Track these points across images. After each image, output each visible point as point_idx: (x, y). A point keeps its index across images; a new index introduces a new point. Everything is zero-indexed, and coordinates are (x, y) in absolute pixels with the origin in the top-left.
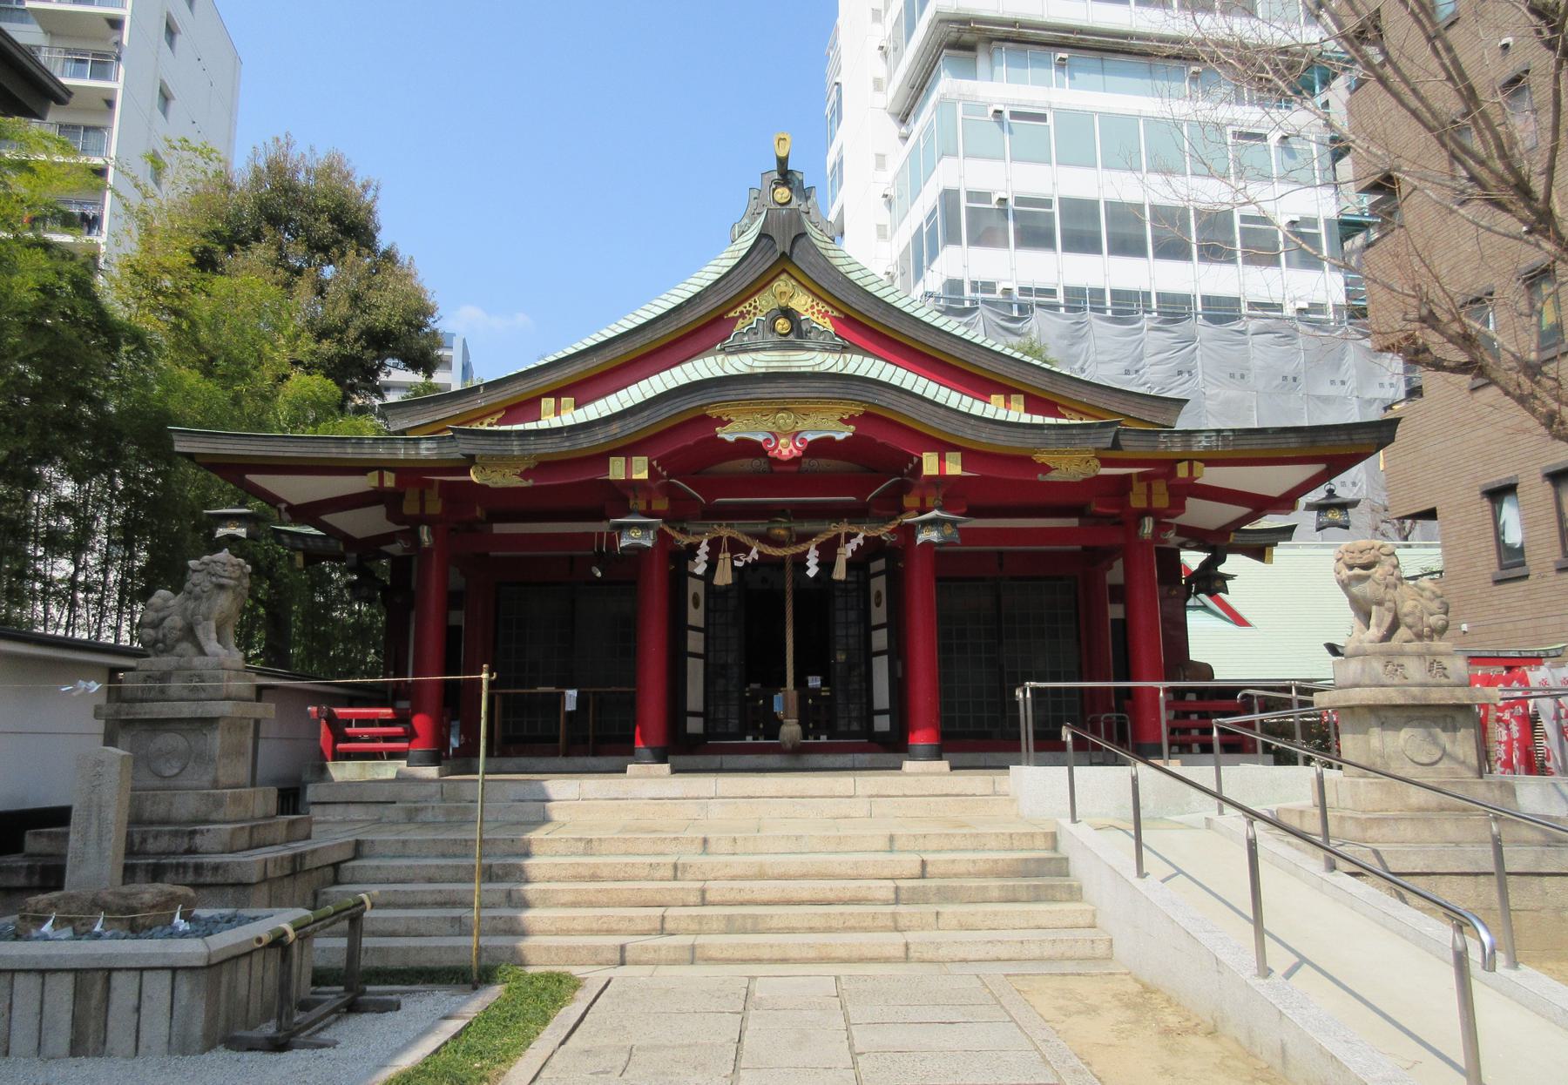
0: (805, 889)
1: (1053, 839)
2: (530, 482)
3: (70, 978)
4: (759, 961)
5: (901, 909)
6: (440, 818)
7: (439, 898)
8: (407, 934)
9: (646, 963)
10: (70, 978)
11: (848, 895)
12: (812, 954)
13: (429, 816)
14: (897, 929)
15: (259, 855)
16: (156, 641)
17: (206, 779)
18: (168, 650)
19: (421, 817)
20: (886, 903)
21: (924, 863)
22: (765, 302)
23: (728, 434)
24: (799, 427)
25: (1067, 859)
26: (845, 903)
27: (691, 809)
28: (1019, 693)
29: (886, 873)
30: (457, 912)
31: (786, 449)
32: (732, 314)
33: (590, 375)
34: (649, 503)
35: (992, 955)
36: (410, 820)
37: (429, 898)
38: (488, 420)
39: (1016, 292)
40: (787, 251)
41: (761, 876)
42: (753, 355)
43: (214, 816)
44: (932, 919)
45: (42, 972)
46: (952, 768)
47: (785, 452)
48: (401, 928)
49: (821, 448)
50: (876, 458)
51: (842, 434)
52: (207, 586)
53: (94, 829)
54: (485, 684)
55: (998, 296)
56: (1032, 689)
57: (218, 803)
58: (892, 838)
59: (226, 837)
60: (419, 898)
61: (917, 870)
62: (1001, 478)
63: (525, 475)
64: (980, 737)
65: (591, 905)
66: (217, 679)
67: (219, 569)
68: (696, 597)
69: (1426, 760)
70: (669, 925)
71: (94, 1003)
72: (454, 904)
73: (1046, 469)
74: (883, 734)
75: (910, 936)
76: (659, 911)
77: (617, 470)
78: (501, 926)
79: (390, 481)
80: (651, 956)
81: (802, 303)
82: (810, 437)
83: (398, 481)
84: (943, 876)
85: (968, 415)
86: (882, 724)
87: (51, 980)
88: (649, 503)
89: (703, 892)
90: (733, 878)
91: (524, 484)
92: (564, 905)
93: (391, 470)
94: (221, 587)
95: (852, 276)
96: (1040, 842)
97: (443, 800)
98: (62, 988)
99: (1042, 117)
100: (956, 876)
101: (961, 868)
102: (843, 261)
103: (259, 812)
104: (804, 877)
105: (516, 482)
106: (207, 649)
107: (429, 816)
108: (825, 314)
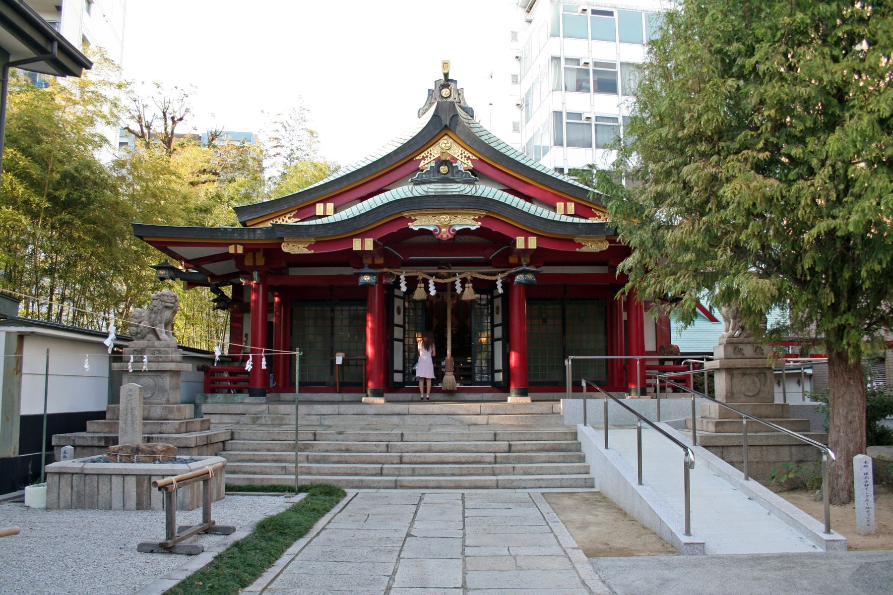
0: (452, 456)
1: (575, 435)
2: (312, 251)
3: (134, 478)
4: (427, 488)
5: (497, 466)
6: (269, 422)
7: (275, 458)
8: (261, 473)
9: (374, 488)
10: (134, 478)
11: (471, 460)
12: (452, 485)
13: (263, 421)
14: (494, 475)
15: (193, 435)
16: (137, 333)
17: (164, 399)
18: (143, 338)
19: (259, 422)
20: (490, 463)
21: (510, 445)
22: (435, 152)
23: (414, 226)
24: (453, 222)
25: (580, 443)
26: (470, 463)
27: (396, 420)
28: (566, 362)
29: (491, 449)
30: (283, 464)
31: (445, 234)
32: (418, 158)
33: (345, 188)
34: (373, 261)
35: (538, 485)
36: (254, 423)
37: (269, 458)
38: (288, 215)
39: (593, 119)
40: (448, 124)
41: (430, 451)
42: (428, 186)
43: (169, 417)
44: (511, 470)
45: (124, 475)
46: (533, 401)
47: (445, 236)
48: (258, 471)
49: (466, 232)
50: (490, 242)
51: (475, 226)
52: (160, 307)
53: (130, 419)
54: (298, 358)
55: (583, 121)
56: (572, 360)
57: (171, 411)
58: (495, 435)
59: (177, 426)
60: (264, 458)
61: (507, 448)
62: (558, 247)
63: (309, 248)
64: (543, 383)
65: (347, 463)
66: (167, 353)
67: (165, 298)
68: (399, 308)
69: (751, 394)
70: (384, 472)
71: (145, 488)
72: (281, 461)
73: (580, 246)
74: (499, 383)
75: (499, 478)
76: (380, 466)
77: (357, 245)
78: (305, 471)
79: (240, 250)
80: (376, 484)
81: (456, 151)
82: (457, 228)
83: (244, 249)
84: (519, 451)
85: (540, 218)
86: (499, 377)
87: (127, 478)
88: (373, 261)
89: (401, 457)
90: (416, 452)
91: (309, 252)
92: (334, 463)
93: (240, 244)
94: (167, 307)
95: (483, 138)
96: (569, 437)
97: (269, 413)
98: (131, 483)
99: (611, 14)
100: (526, 451)
101: (529, 448)
102: (478, 130)
103: (188, 416)
104: (451, 451)
105: (306, 251)
106: (161, 337)
107: (263, 421)
108: (468, 158)
